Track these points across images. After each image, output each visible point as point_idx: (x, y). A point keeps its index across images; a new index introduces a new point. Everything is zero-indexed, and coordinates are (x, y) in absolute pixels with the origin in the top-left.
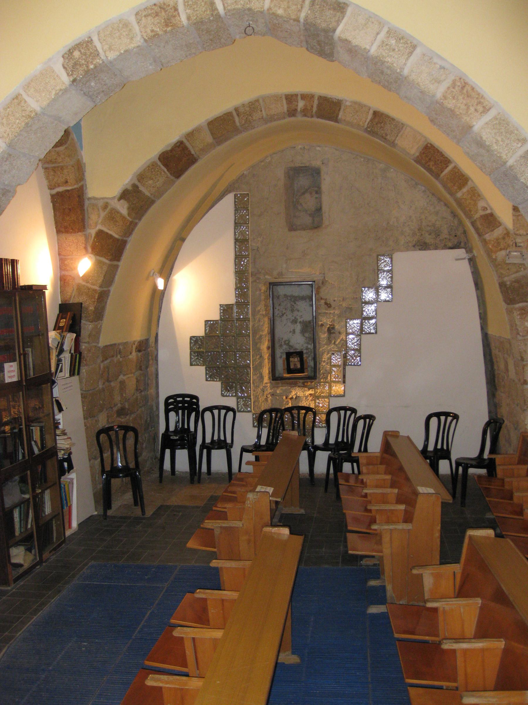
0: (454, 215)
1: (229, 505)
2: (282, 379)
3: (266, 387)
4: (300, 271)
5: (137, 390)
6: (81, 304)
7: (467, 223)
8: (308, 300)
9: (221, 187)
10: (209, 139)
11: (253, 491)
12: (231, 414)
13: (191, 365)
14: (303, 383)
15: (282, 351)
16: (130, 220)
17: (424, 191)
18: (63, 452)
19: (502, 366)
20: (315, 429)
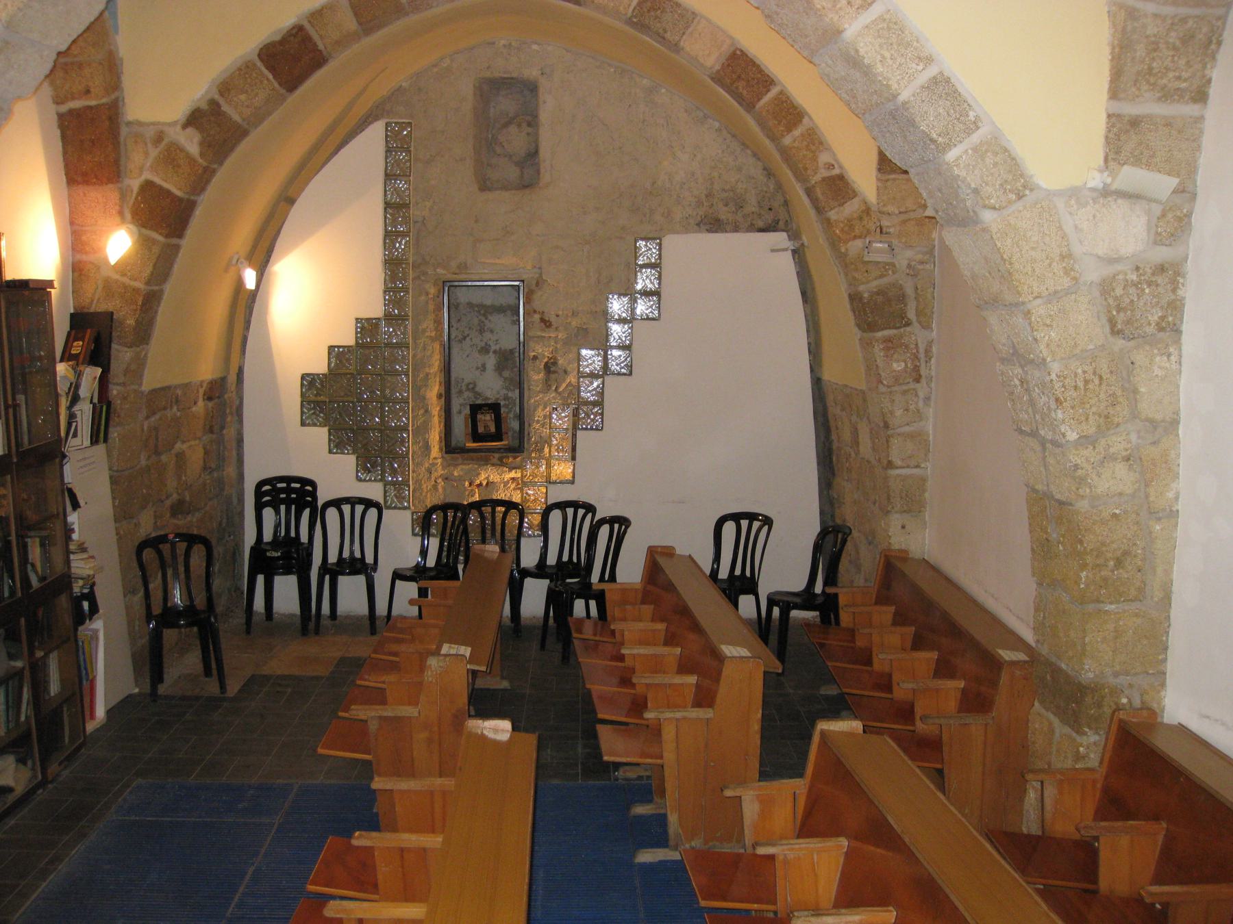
0: (769, 173)
1: (391, 678)
2: (463, 450)
3: (434, 464)
4: (497, 261)
5: (205, 468)
6: (112, 313)
7: (798, 192)
8: (509, 313)
9: (361, 109)
10: (351, 24)
11: (437, 653)
12: (373, 512)
13: (303, 424)
14: (501, 459)
15: (461, 401)
16: (205, 164)
17: (719, 130)
18: (81, 583)
19: (847, 435)
20: (523, 541)
